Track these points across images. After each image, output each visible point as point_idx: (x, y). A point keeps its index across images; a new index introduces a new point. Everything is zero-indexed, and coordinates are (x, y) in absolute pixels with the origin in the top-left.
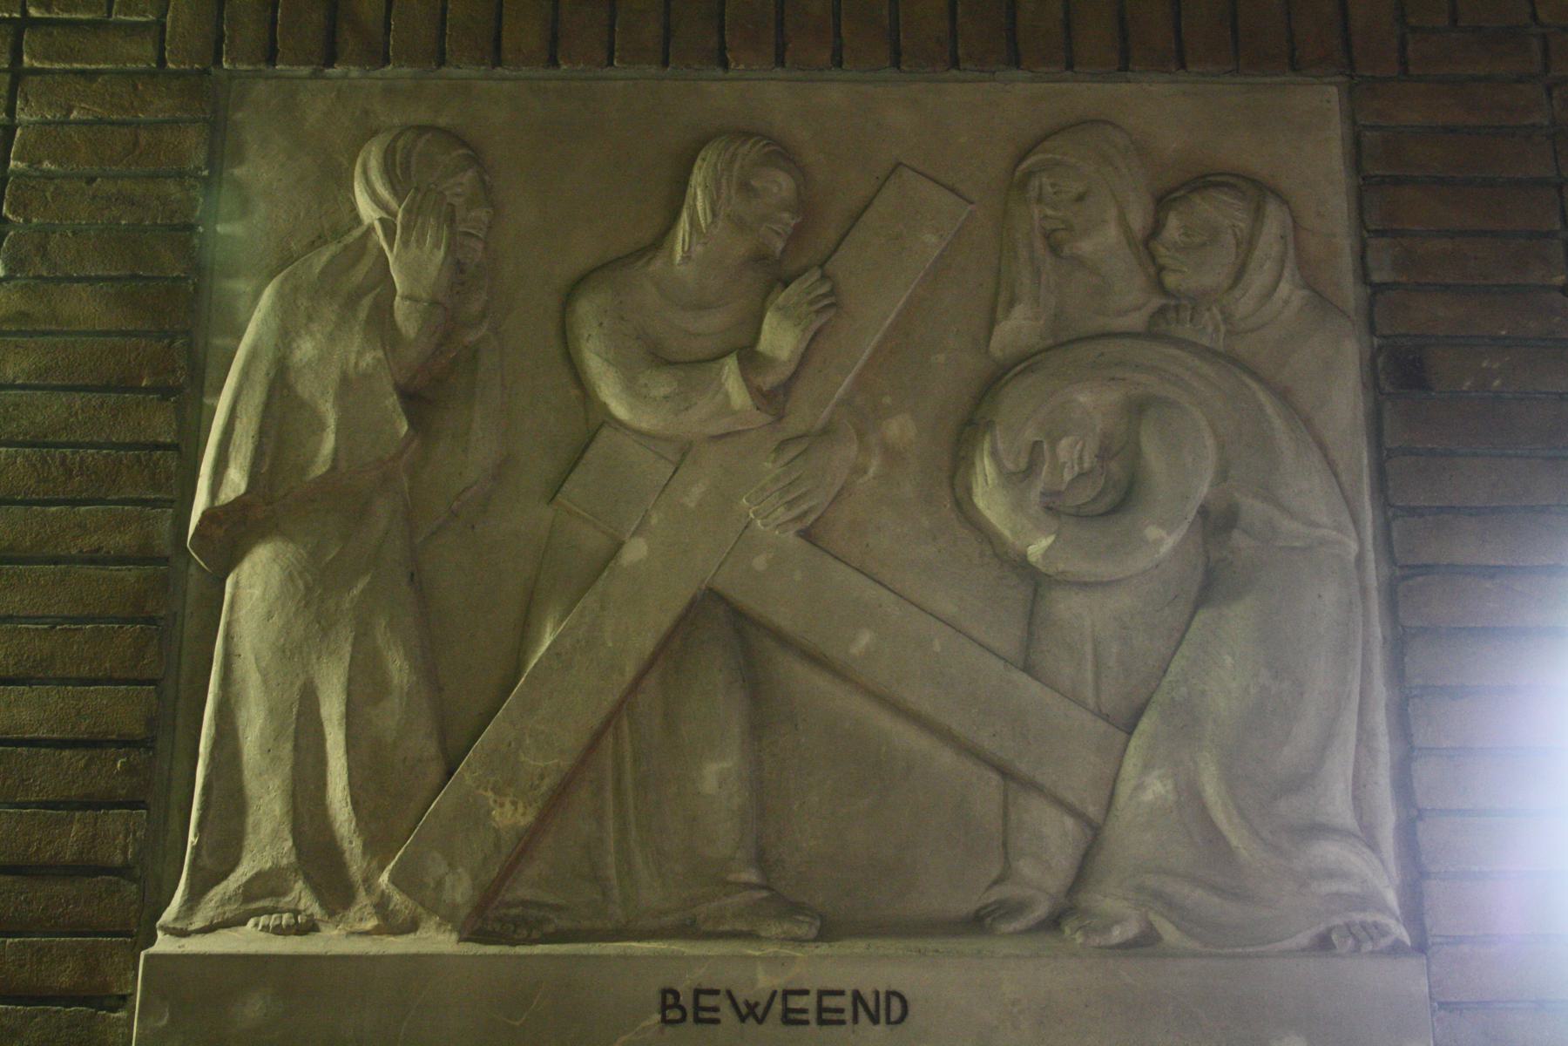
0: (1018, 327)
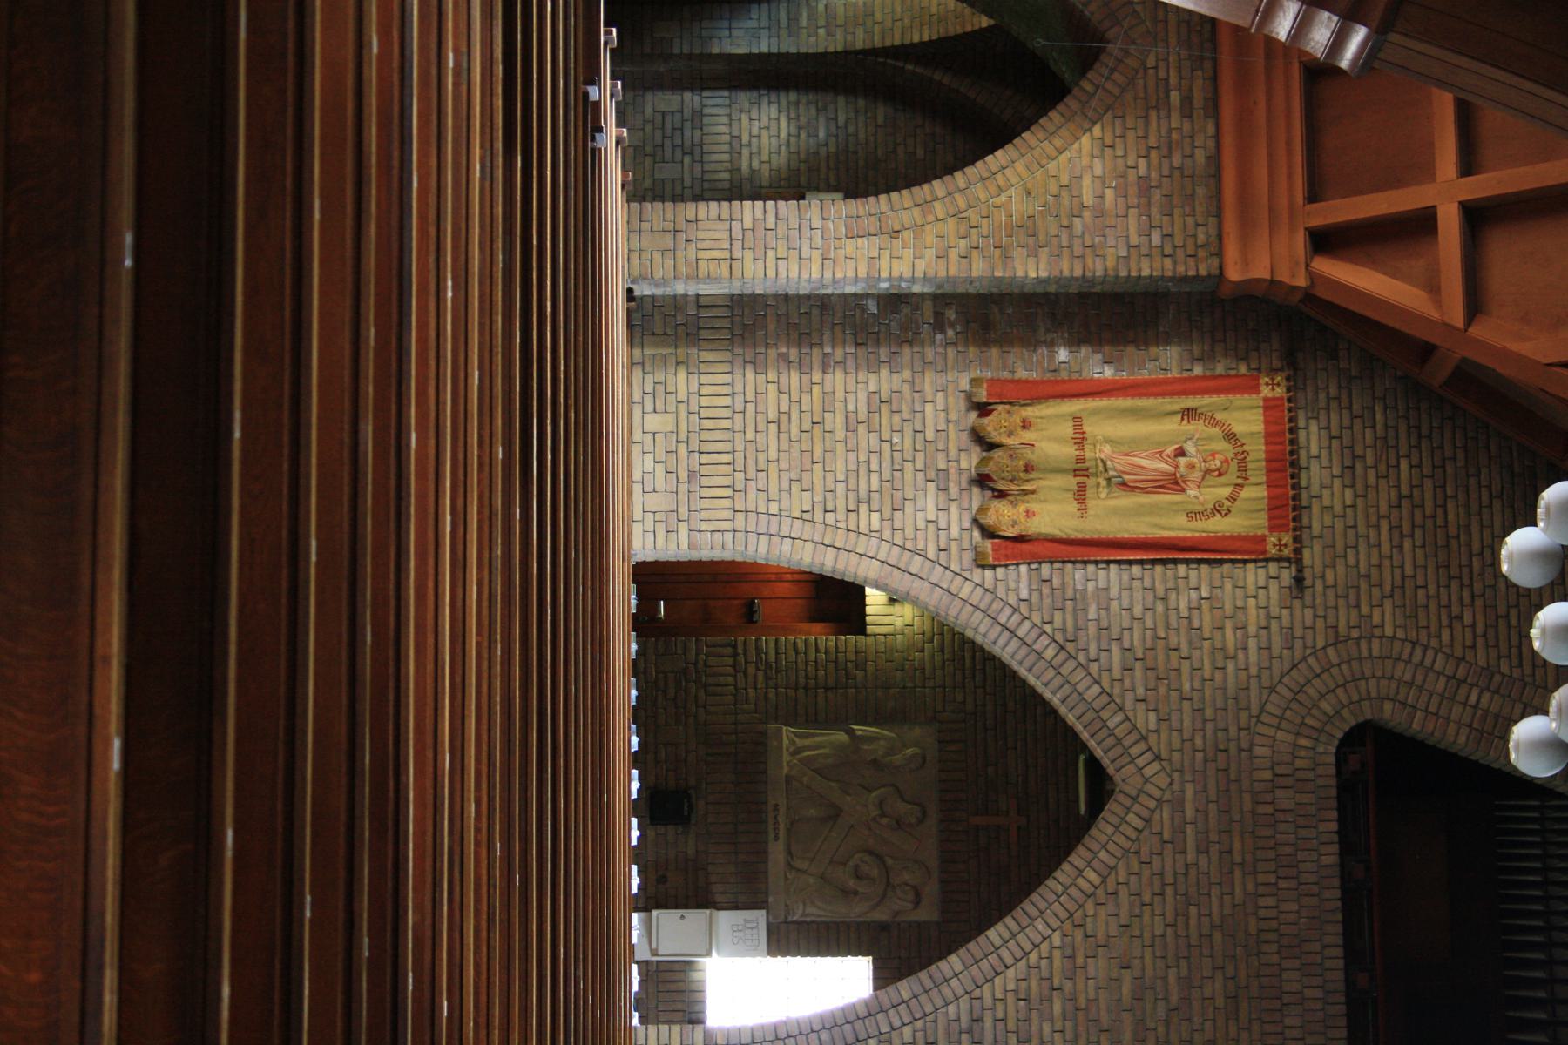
0: (889, 861)
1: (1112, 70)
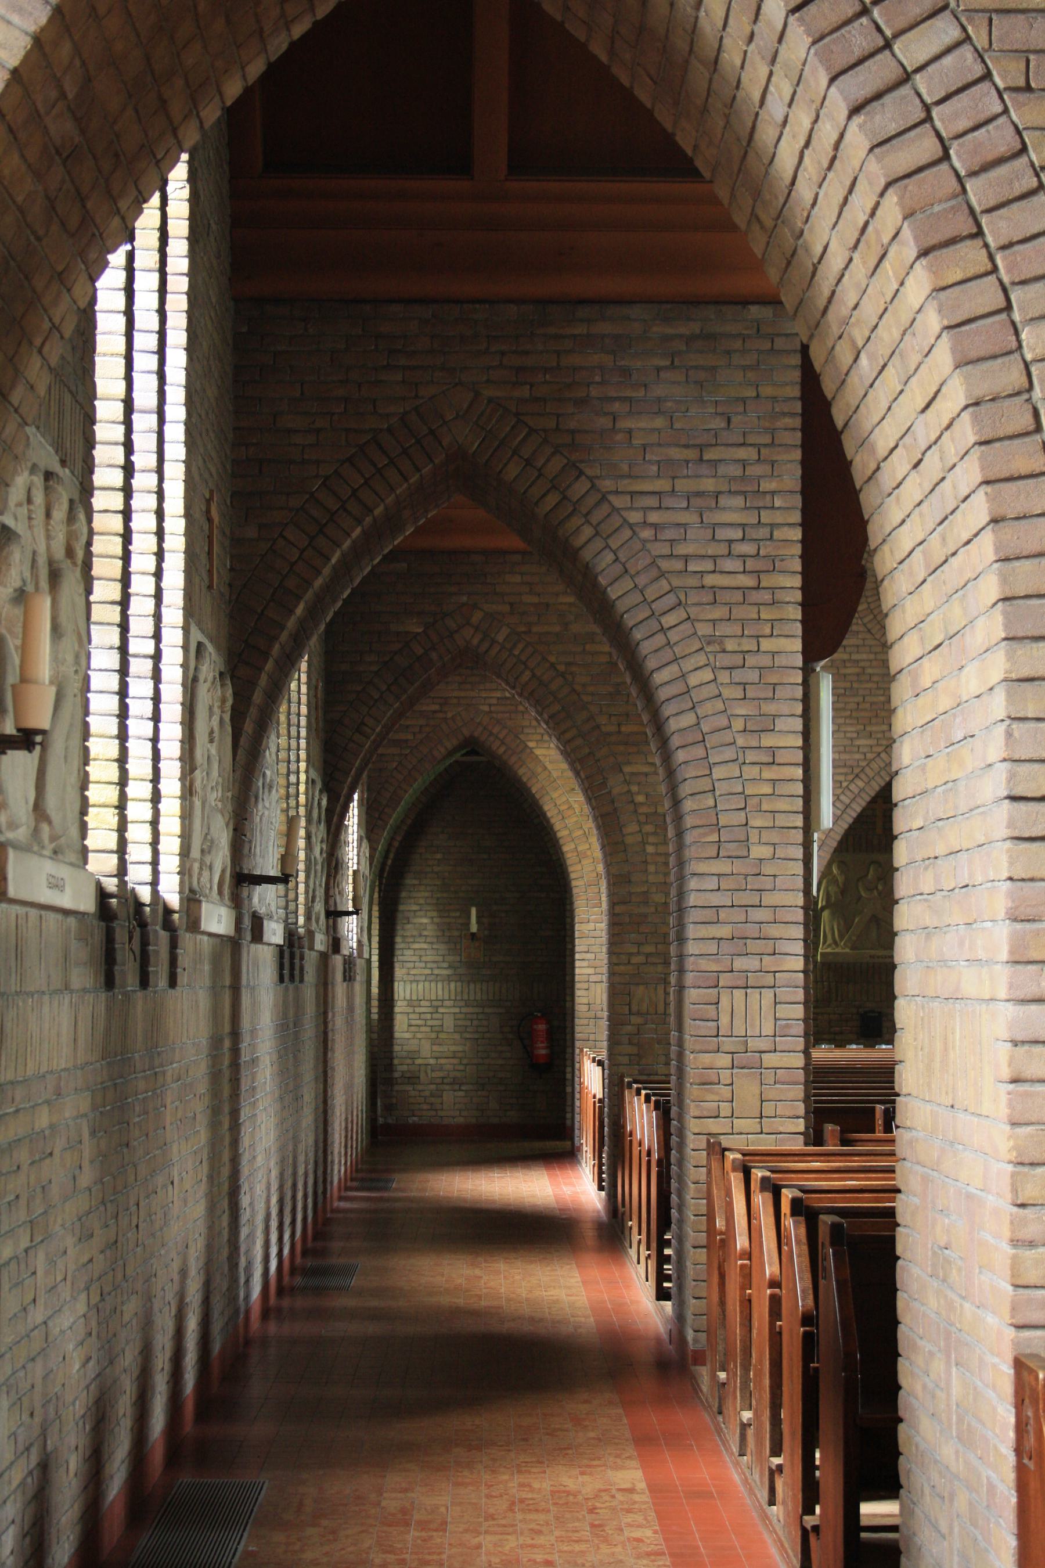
1: (491, 734)
